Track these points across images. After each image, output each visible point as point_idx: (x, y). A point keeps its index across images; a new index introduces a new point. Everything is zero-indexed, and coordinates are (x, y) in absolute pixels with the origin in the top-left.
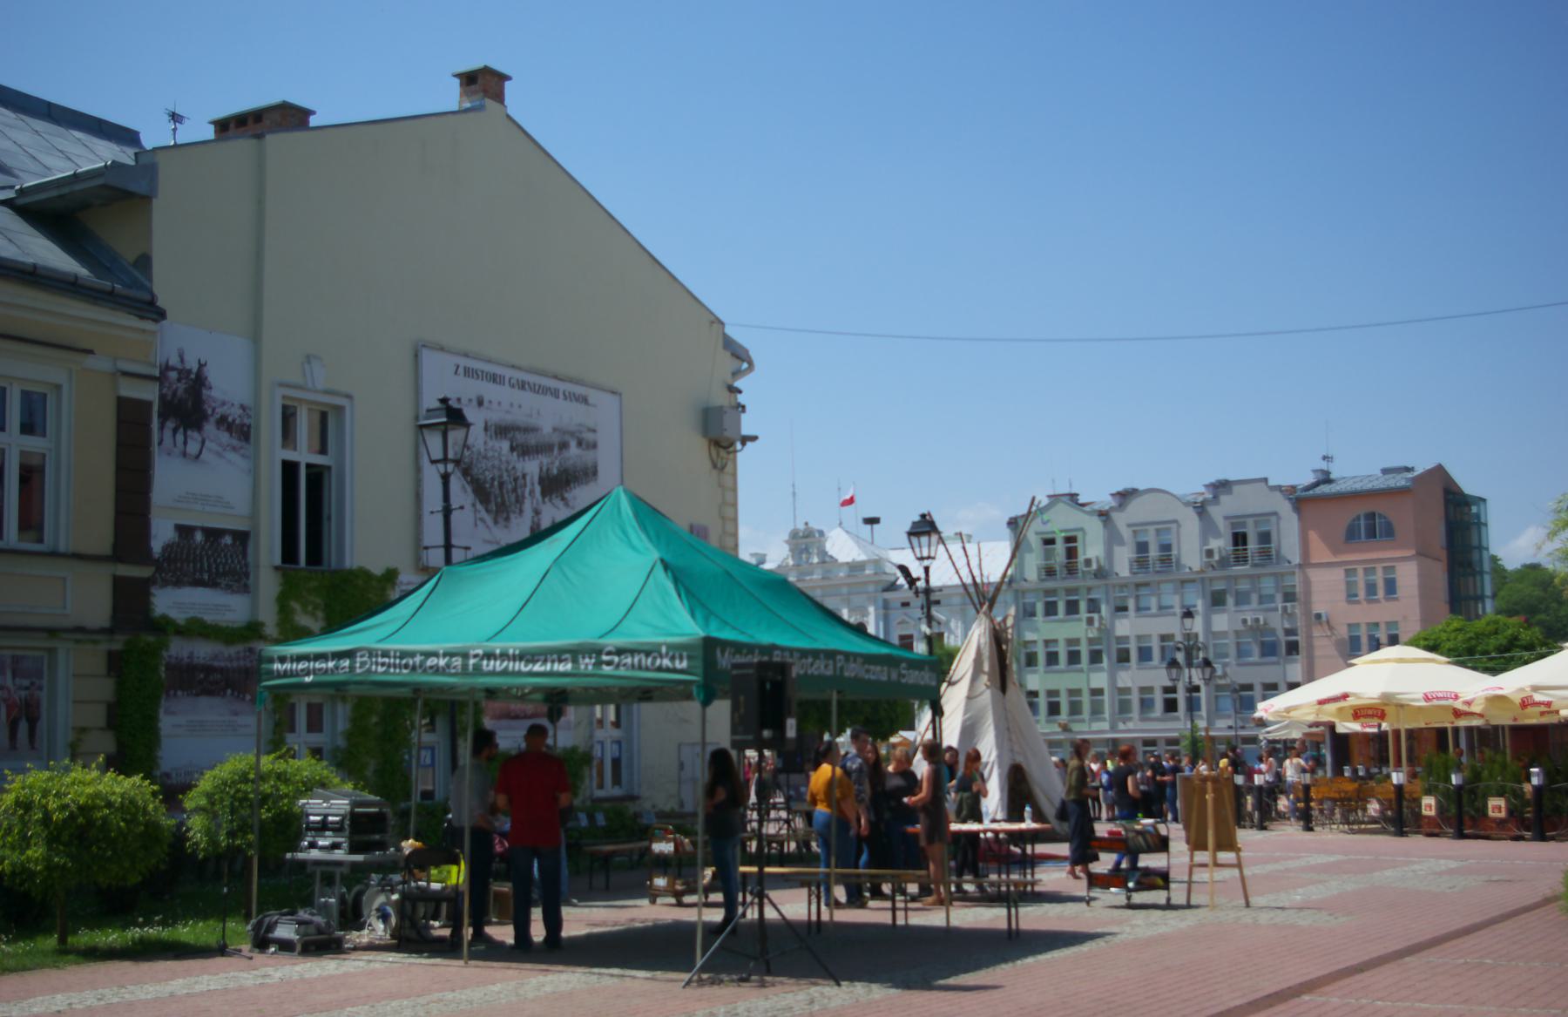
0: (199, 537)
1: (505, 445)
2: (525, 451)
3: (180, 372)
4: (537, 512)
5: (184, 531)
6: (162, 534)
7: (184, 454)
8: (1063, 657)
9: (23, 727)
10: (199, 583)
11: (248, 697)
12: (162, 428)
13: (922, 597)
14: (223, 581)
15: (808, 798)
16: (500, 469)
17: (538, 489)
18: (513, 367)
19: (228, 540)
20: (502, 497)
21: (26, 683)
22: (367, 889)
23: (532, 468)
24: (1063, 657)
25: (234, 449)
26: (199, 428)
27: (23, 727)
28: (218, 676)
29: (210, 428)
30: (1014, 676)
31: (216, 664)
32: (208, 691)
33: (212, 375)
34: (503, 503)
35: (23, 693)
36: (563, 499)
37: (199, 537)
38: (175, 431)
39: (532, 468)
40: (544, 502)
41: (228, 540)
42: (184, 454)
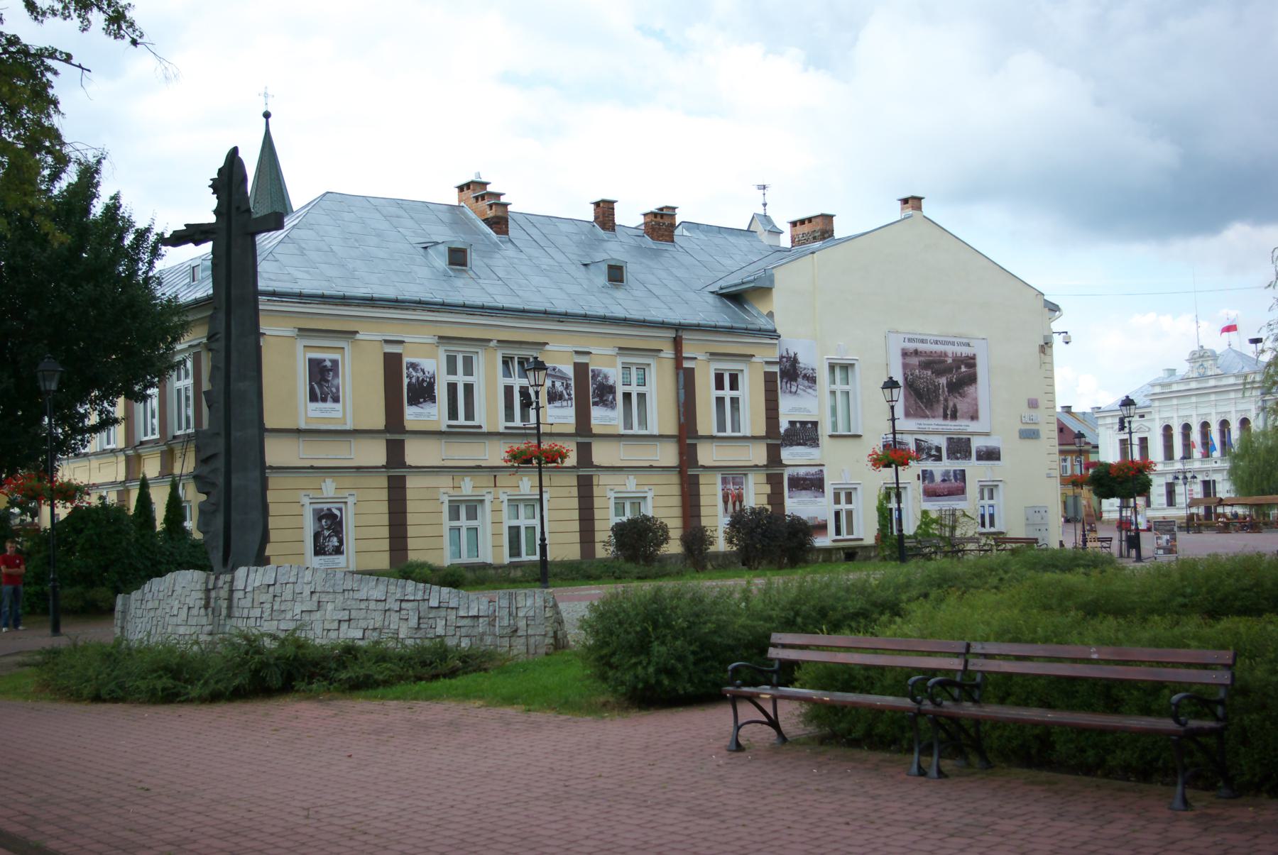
0: (798, 425)
1: (929, 373)
2: (939, 373)
3: (787, 358)
4: (946, 400)
5: (792, 423)
6: (784, 425)
7: (791, 392)
9: (737, 503)
12: (781, 381)
17: (946, 389)
19: (810, 425)
21: (738, 487)
23: (943, 381)
25: (810, 388)
26: (796, 380)
27: (737, 503)
29: (800, 380)
33: (801, 358)
36: (959, 393)
38: (787, 383)
39: (943, 381)
41: (810, 425)
42: (791, 392)
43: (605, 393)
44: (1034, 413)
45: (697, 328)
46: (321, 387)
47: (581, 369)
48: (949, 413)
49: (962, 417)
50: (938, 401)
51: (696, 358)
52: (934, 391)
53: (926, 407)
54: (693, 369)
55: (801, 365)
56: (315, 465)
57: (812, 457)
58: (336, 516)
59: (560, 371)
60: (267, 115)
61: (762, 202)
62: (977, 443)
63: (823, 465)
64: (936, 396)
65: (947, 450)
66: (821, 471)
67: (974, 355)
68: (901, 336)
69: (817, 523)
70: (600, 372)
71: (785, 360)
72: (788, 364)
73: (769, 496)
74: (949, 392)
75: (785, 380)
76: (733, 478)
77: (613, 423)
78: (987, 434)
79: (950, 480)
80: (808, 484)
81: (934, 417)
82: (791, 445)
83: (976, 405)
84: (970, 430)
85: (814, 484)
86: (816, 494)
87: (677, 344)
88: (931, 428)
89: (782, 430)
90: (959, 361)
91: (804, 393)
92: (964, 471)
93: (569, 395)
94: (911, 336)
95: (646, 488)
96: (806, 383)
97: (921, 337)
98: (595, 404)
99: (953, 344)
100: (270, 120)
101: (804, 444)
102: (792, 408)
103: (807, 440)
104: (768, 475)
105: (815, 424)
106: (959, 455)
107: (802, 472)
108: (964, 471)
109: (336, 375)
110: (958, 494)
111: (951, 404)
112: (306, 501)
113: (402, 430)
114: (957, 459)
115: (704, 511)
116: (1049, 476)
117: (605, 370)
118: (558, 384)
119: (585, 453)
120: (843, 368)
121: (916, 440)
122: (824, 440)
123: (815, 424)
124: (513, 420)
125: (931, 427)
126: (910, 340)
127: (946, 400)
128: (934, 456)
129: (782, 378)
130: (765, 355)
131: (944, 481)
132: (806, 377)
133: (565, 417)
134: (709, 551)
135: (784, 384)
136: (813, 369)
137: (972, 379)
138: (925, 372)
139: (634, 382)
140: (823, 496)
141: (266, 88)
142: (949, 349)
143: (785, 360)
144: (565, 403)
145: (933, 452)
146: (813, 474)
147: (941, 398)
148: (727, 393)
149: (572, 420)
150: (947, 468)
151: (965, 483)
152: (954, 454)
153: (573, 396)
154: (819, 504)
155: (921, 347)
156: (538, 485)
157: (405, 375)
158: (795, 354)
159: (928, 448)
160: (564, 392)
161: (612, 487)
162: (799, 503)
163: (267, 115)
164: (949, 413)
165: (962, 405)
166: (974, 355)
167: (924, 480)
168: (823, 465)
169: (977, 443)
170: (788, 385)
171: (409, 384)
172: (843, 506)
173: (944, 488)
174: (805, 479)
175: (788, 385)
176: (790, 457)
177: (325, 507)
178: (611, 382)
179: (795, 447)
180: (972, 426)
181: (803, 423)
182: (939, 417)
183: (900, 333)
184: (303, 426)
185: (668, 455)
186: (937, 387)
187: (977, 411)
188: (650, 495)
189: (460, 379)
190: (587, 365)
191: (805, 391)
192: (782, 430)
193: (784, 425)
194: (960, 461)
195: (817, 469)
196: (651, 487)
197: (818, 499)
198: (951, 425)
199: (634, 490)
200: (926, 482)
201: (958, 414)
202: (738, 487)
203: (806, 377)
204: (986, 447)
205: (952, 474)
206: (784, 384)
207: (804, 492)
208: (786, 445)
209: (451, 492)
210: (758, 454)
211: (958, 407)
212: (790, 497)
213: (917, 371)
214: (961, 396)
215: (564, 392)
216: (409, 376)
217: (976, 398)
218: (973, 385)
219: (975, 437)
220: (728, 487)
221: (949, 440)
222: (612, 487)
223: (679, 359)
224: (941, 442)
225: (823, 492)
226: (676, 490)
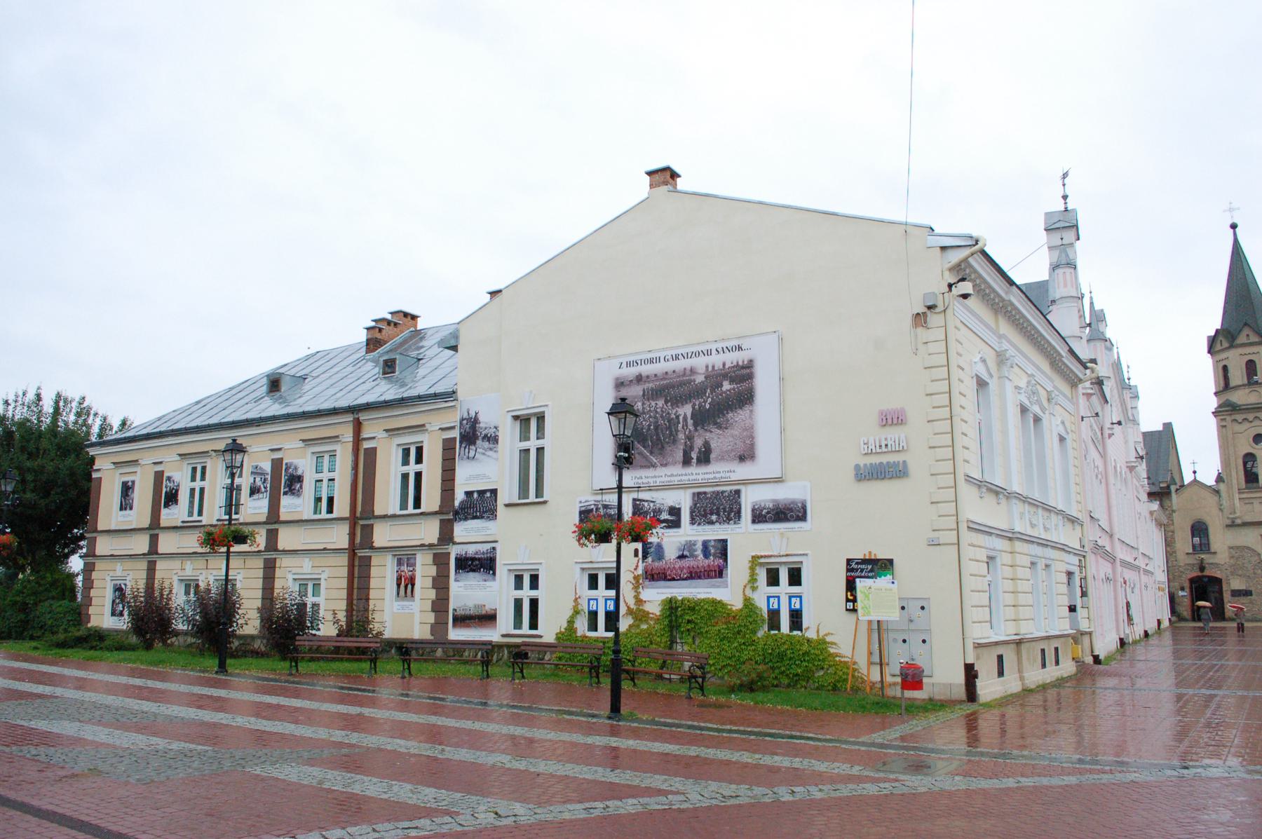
0: (475, 495)
1: (661, 403)
2: (677, 401)
3: (467, 419)
4: (690, 438)
5: (469, 494)
6: (459, 497)
7: (468, 458)
8: (784, 576)
9: (410, 586)
10: (475, 518)
11: (491, 572)
12: (460, 446)
13: (48, 610)
14: (485, 515)
15: (1232, 561)
16: (655, 417)
17: (690, 422)
18: (698, 344)
19: (488, 494)
20: (657, 435)
21: (411, 569)
22: (1207, 536)
23: (686, 410)
24: (784, 576)
25: (491, 449)
26: (474, 443)
27: (410, 586)
28: (477, 562)
29: (479, 442)
30: (441, 645)
31: (477, 556)
32: (474, 570)
33: (481, 418)
34: (659, 439)
35: (410, 573)
36: (715, 423)
37: (475, 495)
38: (465, 448)
39: (686, 410)
40: (696, 430)
41: (488, 494)
42: (468, 458)
43: (295, 481)
44: (893, 435)
45: (368, 407)
46: (125, 499)
47: (277, 464)
48: (694, 455)
49: (722, 458)
50: (675, 441)
51: (374, 438)
52: (669, 428)
53: (651, 453)
54: (375, 449)
55: (481, 425)
56: (328, 547)
57: (489, 532)
58: (122, 589)
59: (261, 468)
60: (1234, 226)
61: (1062, 194)
62: (751, 498)
63: (496, 542)
64: (671, 434)
65: (692, 512)
66: (494, 548)
67: (751, 361)
68: (616, 362)
69: (484, 612)
70: (291, 464)
71: (465, 422)
72: (468, 426)
73: (434, 579)
74: (696, 425)
75: (463, 445)
76: (408, 559)
77: (299, 509)
78: (779, 480)
79: (695, 557)
80: (477, 565)
81: (665, 465)
82: (466, 519)
83: (752, 437)
84: (734, 477)
85: (483, 564)
86: (486, 577)
87: (358, 426)
88: (659, 481)
89: (457, 503)
90: (718, 375)
91: (483, 457)
92: (724, 542)
93: (265, 488)
94: (631, 359)
95: (320, 570)
96: (486, 444)
97: (649, 356)
98: (285, 493)
99: (709, 353)
100: (1237, 230)
101: (482, 517)
102: (469, 477)
103: (484, 512)
104: (435, 555)
105: (494, 492)
106: (714, 517)
107: (471, 550)
108: (724, 542)
109: (133, 492)
110: (709, 577)
111: (698, 442)
112: (108, 579)
113: (278, 522)
114: (712, 523)
115: (372, 594)
116: (934, 544)
117: (296, 461)
118: (258, 479)
119: (272, 536)
120: (530, 422)
121: (634, 500)
122: (501, 510)
123: (494, 492)
124: (406, 508)
125: (658, 480)
126: (629, 364)
127: (690, 438)
128: (665, 521)
129: (461, 443)
130: (449, 419)
131: (682, 557)
132: (487, 438)
133: (260, 508)
134: (89, 625)
135: (462, 449)
136: (496, 428)
137: (746, 398)
138: (653, 404)
139: (326, 468)
140: (494, 580)
141: (1231, 203)
142: (700, 363)
143: (465, 422)
144: (261, 496)
145: (665, 516)
146: (483, 553)
147: (681, 436)
148: (412, 468)
149: (266, 510)
150: (689, 539)
151: (726, 560)
152: (705, 516)
153: (268, 489)
154: (488, 589)
155: (646, 369)
156: (615, 559)
157: (164, 486)
158: (476, 414)
159: (654, 511)
160: (262, 486)
161: (290, 569)
162: (466, 587)
163: (1234, 226)
164: (694, 455)
165: (718, 440)
166: (751, 361)
167: (645, 557)
168: (496, 542)
169: (751, 498)
170: (467, 450)
171: (166, 492)
172: (526, 593)
173: (681, 569)
174: (473, 559)
175: (467, 450)
176: (464, 533)
177: (118, 582)
178: (299, 472)
179: (470, 522)
180: (742, 471)
181: (481, 493)
182: (675, 463)
183: (615, 357)
184: (113, 527)
185: (339, 537)
186: (672, 423)
187: (752, 447)
188: (323, 576)
189: (198, 484)
190: (281, 459)
191: (484, 454)
192: (457, 503)
193: (459, 497)
194: (717, 525)
195: (488, 546)
196: (323, 569)
197: (488, 583)
198: (698, 474)
199: (309, 572)
200: (650, 559)
201: (713, 456)
202: (411, 569)
203: (487, 438)
204: (773, 501)
205: (699, 546)
206: (462, 449)
207: (472, 574)
208: (460, 520)
209: (181, 573)
210: (429, 532)
211: (713, 445)
212: (456, 580)
213: (640, 404)
214: (720, 427)
215: (262, 486)
216: (166, 487)
217: (752, 427)
218: (747, 408)
219: (750, 488)
220: (402, 568)
221: (698, 497)
222: (290, 569)
223: (357, 440)
224: (684, 501)
225: (494, 574)
226: (344, 572)
